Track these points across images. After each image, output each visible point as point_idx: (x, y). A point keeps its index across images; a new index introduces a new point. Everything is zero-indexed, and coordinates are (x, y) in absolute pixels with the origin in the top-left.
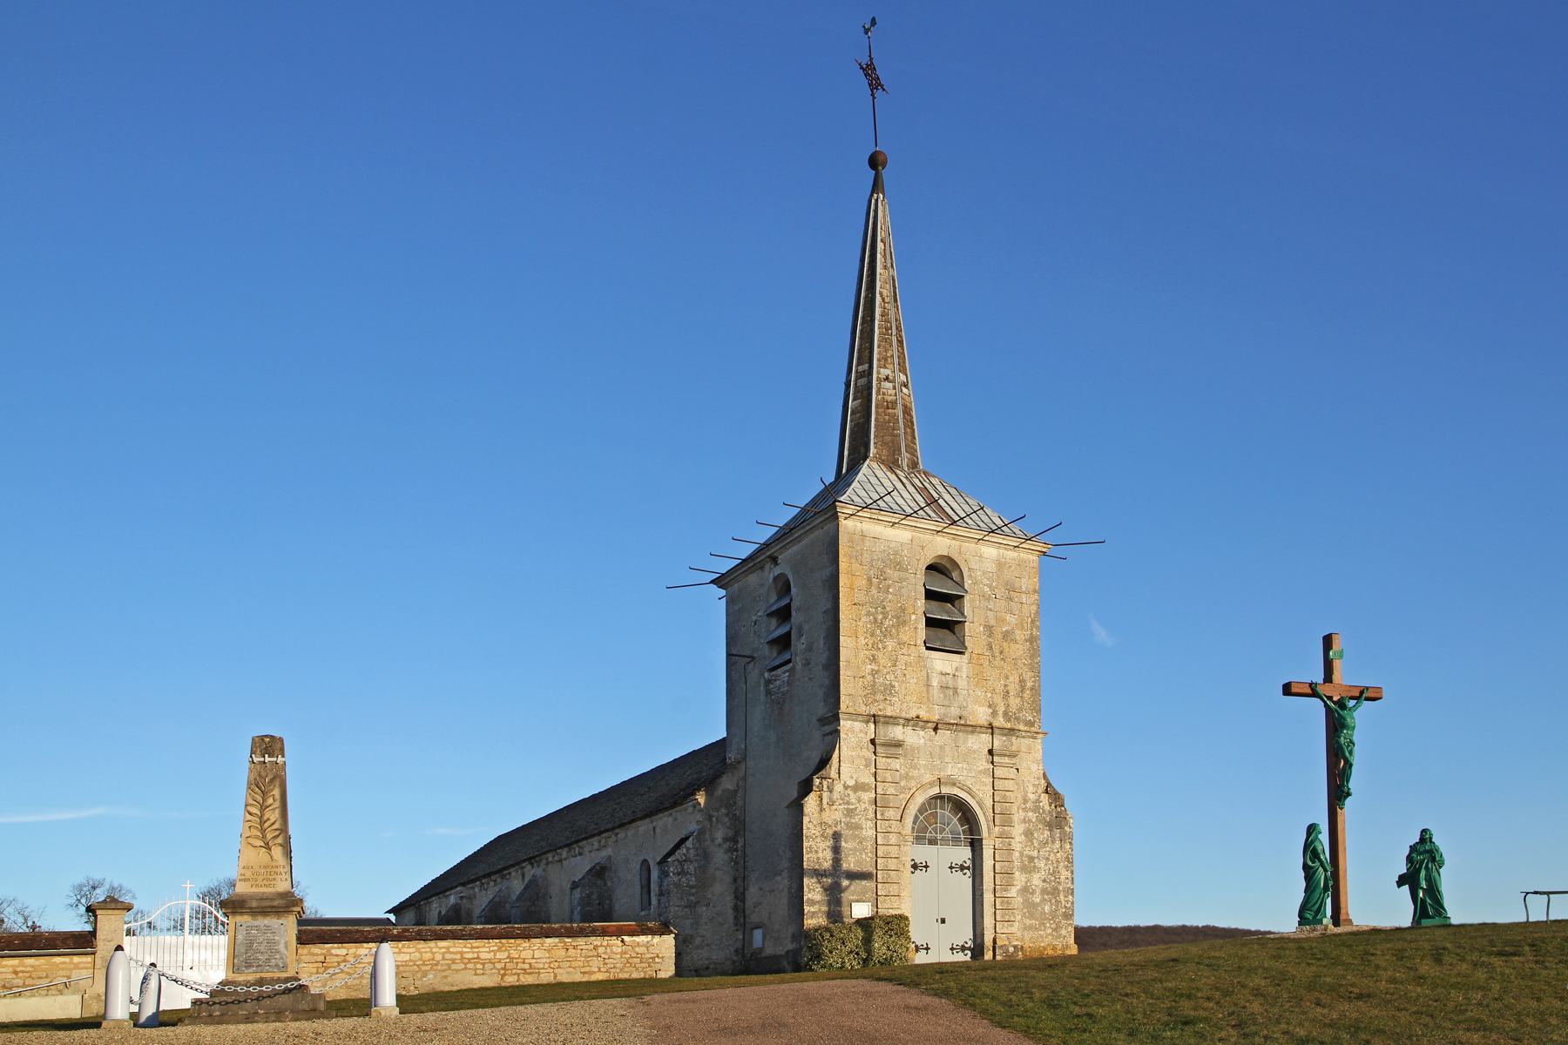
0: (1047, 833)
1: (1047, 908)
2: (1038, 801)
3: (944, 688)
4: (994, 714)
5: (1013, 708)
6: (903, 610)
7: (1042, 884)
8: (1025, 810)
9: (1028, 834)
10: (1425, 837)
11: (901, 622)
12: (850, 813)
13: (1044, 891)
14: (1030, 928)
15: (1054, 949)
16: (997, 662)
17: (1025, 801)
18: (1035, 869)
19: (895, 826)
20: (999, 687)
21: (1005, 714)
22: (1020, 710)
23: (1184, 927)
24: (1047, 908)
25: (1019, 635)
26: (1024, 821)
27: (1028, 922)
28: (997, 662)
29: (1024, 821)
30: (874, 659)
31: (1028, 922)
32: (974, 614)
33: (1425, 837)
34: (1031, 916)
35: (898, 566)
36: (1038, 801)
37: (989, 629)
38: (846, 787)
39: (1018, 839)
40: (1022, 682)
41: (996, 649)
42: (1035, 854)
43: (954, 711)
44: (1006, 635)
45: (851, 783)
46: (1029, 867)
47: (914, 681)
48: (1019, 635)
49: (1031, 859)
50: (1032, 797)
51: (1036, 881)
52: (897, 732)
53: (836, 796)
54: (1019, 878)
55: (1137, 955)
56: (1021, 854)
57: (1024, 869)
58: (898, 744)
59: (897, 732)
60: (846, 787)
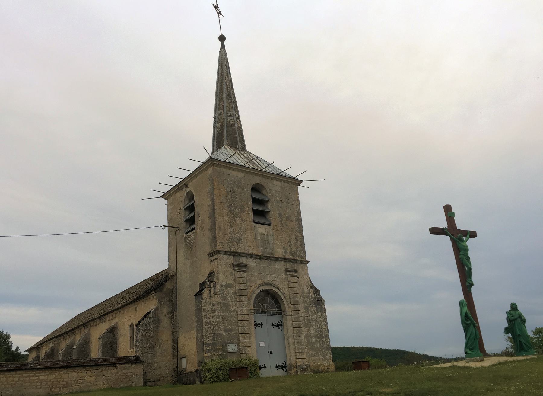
0: (314, 308)
3: (263, 240)
4: (286, 252)
8: (303, 297)
9: (306, 308)
12: (224, 298)
13: (316, 337)
14: (312, 355)
15: (324, 366)
22: (297, 251)
30: (231, 227)
31: (311, 352)
38: (222, 286)
45: (224, 284)
46: (308, 325)
49: (309, 320)
51: (312, 331)
52: (243, 260)
54: (304, 330)
58: (245, 266)
59: (243, 260)
60: (222, 286)
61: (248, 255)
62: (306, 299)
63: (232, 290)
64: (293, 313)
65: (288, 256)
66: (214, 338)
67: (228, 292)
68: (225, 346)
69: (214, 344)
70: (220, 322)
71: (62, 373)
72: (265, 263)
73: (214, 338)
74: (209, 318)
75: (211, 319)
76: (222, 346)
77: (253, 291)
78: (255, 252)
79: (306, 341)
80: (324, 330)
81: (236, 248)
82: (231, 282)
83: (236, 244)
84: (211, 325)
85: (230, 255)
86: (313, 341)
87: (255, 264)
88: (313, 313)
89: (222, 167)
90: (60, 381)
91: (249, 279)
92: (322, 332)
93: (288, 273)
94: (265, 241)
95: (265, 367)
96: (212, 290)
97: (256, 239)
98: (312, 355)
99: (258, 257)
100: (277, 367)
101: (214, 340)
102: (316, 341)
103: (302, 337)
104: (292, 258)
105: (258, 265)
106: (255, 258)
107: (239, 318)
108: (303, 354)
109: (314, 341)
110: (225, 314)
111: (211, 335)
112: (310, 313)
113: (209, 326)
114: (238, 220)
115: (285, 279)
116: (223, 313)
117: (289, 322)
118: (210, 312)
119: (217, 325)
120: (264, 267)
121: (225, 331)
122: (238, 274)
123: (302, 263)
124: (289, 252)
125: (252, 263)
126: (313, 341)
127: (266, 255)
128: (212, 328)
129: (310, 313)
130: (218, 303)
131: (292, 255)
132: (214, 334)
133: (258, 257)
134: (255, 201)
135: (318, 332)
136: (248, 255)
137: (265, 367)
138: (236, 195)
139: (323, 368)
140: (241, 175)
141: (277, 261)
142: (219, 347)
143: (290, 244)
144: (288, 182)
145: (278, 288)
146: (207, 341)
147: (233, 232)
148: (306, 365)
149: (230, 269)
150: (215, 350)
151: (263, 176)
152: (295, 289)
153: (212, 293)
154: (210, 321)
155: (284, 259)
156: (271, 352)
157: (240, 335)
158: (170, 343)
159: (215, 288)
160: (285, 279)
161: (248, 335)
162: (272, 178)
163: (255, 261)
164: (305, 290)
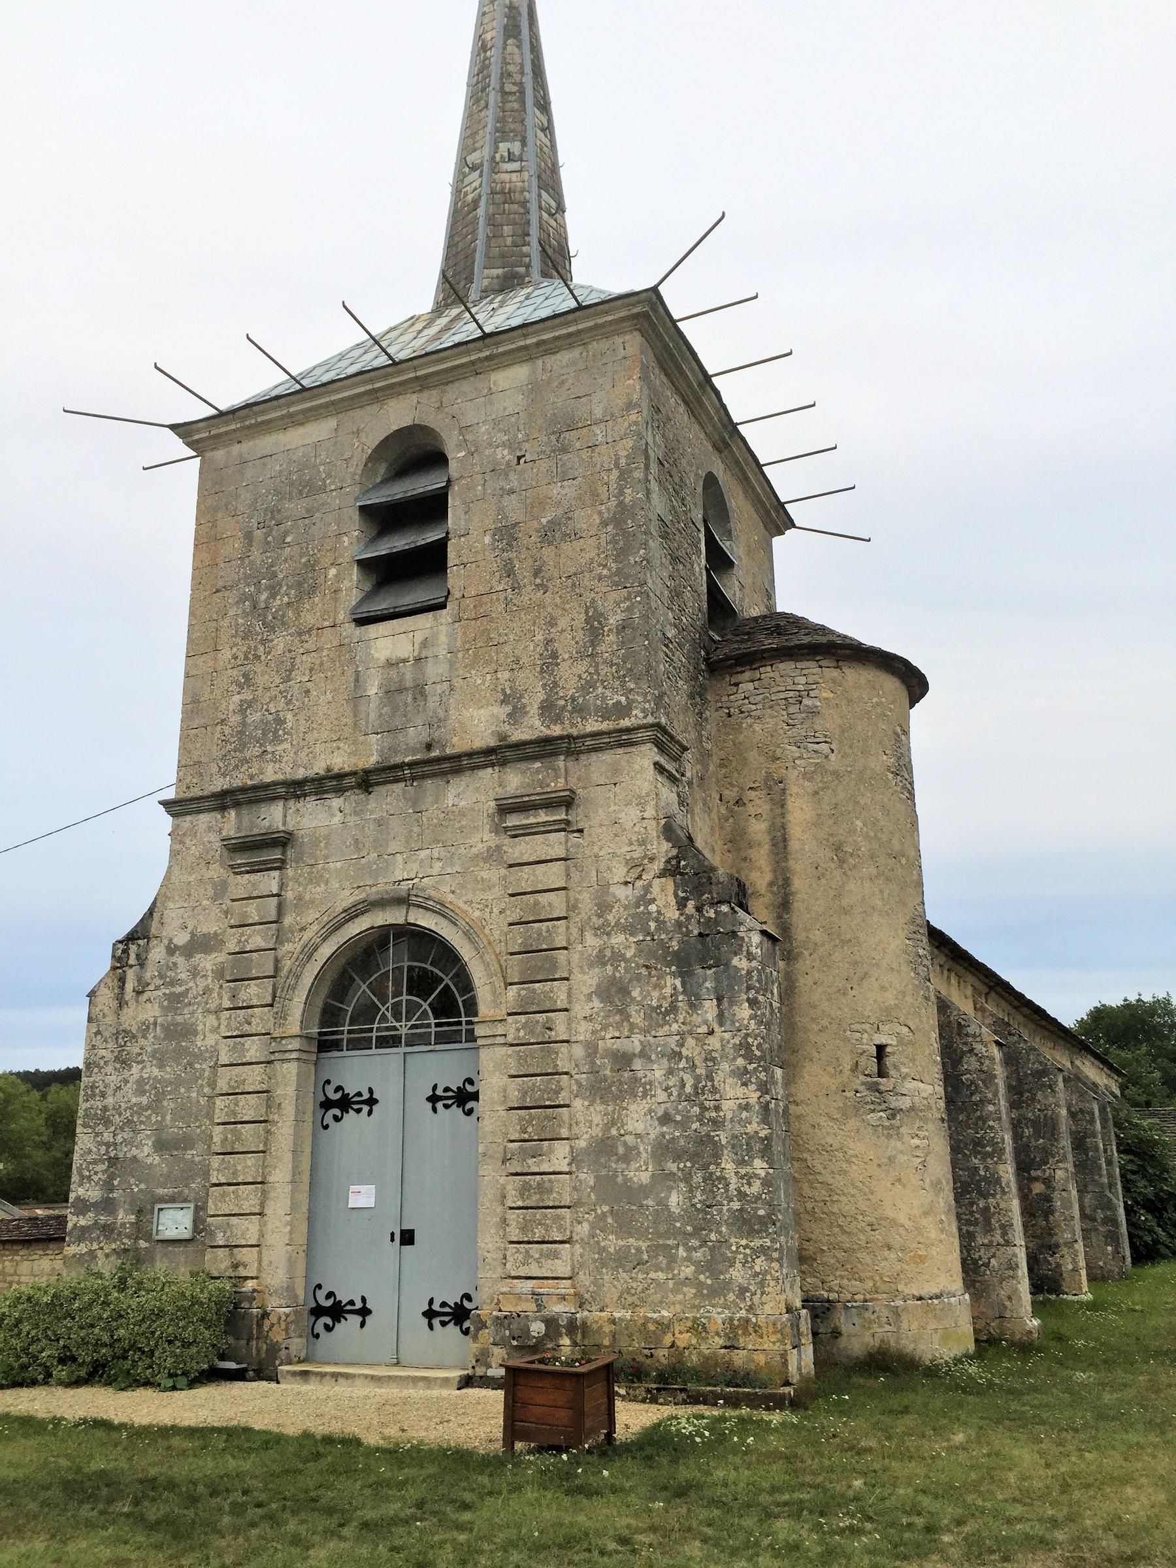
0: (672, 983)
1: (675, 1200)
2: (645, 899)
3: (392, 692)
4: (517, 715)
5: (569, 687)
6: (311, 566)
7: (655, 1130)
8: (603, 930)
9: (614, 993)
10: (160, 803)
11: (306, 585)
12: (175, 1002)
13: (664, 1150)
14: (621, 1260)
15: (698, 1328)
16: (529, 595)
17: (603, 907)
18: (636, 1088)
19: (261, 1020)
20: (531, 651)
21: (548, 709)
22: (588, 686)
23: (1044, 1011)
24: (675, 1200)
25: (586, 519)
26: (600, 960)
27: (612, 1243)
28: (529, 595)
29: (600, 960)
30: (248, 681)
31: (612, 1243)
32: (468, 530)
33: (160, 803)
34: (625, 1226)
35: (310, 488)
36: (645, 899)
37: (507, 534)
38: (171, 950)
39: (581, 1009)
40: (594, 627)
41: (523, 571)
42: (635, 1044)
43: (415, 735)
44: (548, 535)
45: (181, 939)
46: (615, 1080)
47: (326, 701)
48: (586, 519)
49: (623, 1060)
50: (623, 894)
51: (638, 1119)
52: (274, 817)
53: (150, 972)
54: (586, 1119)
55: (694, 363)
56: (591, 1049)
57: (598, 1090)
58: (283, 841)
59: (274, 817)
60: (171, 950)
61: (296, 789)
62: (618, 939)
63: (208, 962)
64: (513, 1028)
65: (532, 727)
66: (112, 1177)
67: (194, 972)
68: (144, 1211)
69: (107, 1205)
70: (142, 1109)
71: (17, 1258)
72: (388, 800)
73: (112, 1177)
74: (103, 1095)
75: (110, 1101)
76: (140, 1211)
77: (310, 952)
78: (341, 761)
79: (587, 1177)
80: (728, 1106)
81: (253, 771)
82: (210, 926)
83: (257, 751)
84: (107, 1122)
85: (223, 808)
86: (641, 1174)
87: (338, 817)
88: (663, 1014)
89: (234, 438)
90: (11, 1283)
91: (300, 898)
92: (717, 1124)
93: (513, 820)
94: (407, 689)
95: (364, 1312)
96: (131, 974)
97: (357, 698)
98: (621, 1260)
99: (347, 781)
100: (430, 1314)
101: (108, 1186)
102: (663, 1178)
103: (559, 1157)
104: (557, 730)
105: (352, 820)
106: (340, 791)
107: (222, 1085)
108: (556, 1256)
109: (645, 1177)
110: (168, 1073)
111: (101, 1167)
112: (637, 1018)
113: (101, 1128)
114: (280, 642)
115: (493, 855)
116: (161, 1066)
117: (495, 1073)
118: (109, 1069)
119: (129, 1122)
120: (380, 823)
121: (161, 1146)
122: (242, 884)
123: (610, 746)
124: (534, 710)
125: (311, 818)
126: (641, 1174)
127: (398, 759)
128: (107, 1137)
129: (637, 1018)
130: (145, 1028)
131: (558, 719)
132: (113, 1161)
133: (352, 781)
134: (383, 518)
135: (683, 1125)
136: (296, 789)
137: (364, 1312)
138: (286, 534)
139: (683, 1339)
140: (320, 430)
141: (457, 771)
142: (124, 1217)
143: (550, 661)
144: (570, 341)
145: (441, 910)
146: (81, 1191)
147: (250, 704)
148: (551, 1323)
149: (217, 872)
150: (108, 1231)
151: (422, 384)
152: (543, 899)
153: (129, 986)
154: (105, 1109)
155: (500, 754)
156: (408, 1238)
157: (216, 1161)
158: (926, 1089)
159: (142, 962)
160: (493, 855)
161: (250, 1160)
162: (474, 370)
163: (336, 802)
164: (623, 894)
